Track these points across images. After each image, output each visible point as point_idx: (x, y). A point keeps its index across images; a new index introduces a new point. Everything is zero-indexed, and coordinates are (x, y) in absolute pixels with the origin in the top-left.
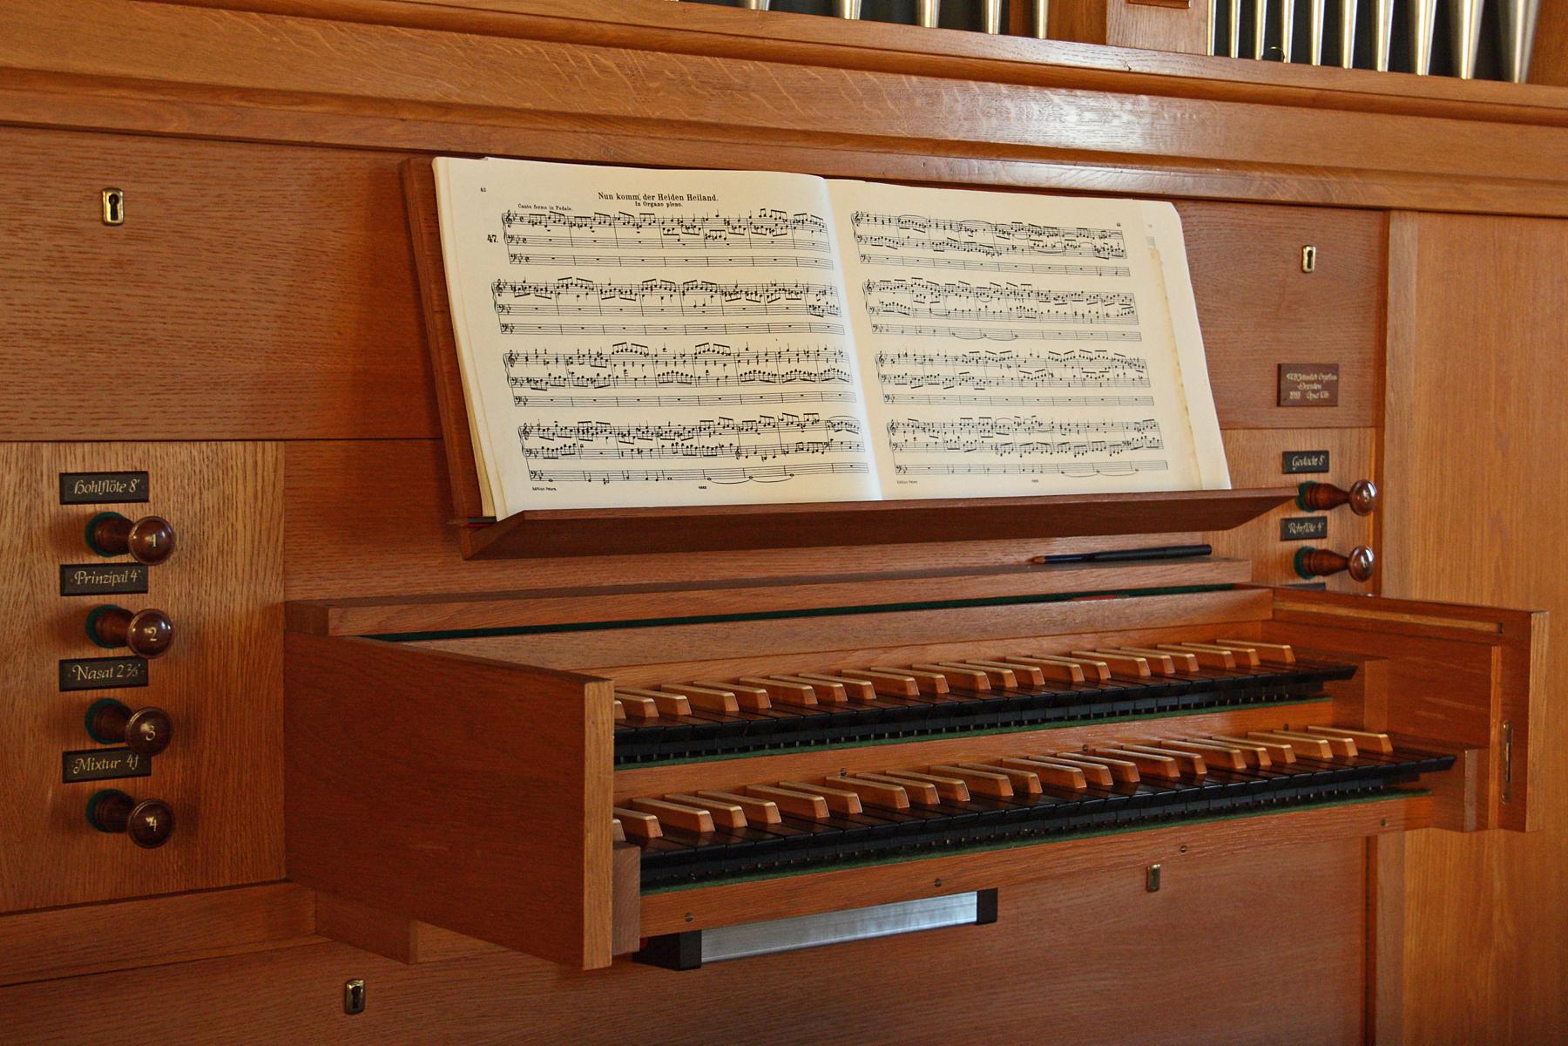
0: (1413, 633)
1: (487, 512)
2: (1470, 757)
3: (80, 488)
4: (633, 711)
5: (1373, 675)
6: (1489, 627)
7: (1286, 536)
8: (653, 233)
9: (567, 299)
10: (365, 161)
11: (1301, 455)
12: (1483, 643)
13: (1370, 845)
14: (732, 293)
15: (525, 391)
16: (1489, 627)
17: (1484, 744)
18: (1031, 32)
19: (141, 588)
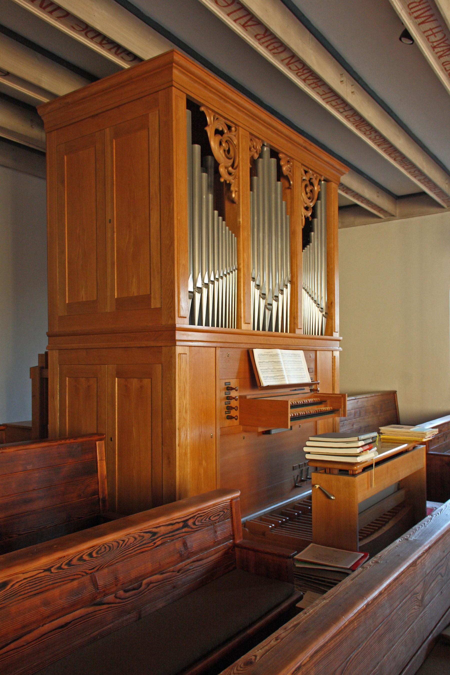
0: (332, 397)
1: (262, 385)
2: (340, 409)
3: (227, 384)
4: (292, 403)
5: (328, 402)
6: (341, 396)
7: (225, 394)
8: (268, 356)
9: (264, 363)
10: (241, 349)
11: (227, 383)
12: (340, 398)
13: (316, 422)
14: (275, 362)
15: (287, 372)
16: (341, 396)
17: (341, 408)
18: (202, 325)
19: (230, 394)
